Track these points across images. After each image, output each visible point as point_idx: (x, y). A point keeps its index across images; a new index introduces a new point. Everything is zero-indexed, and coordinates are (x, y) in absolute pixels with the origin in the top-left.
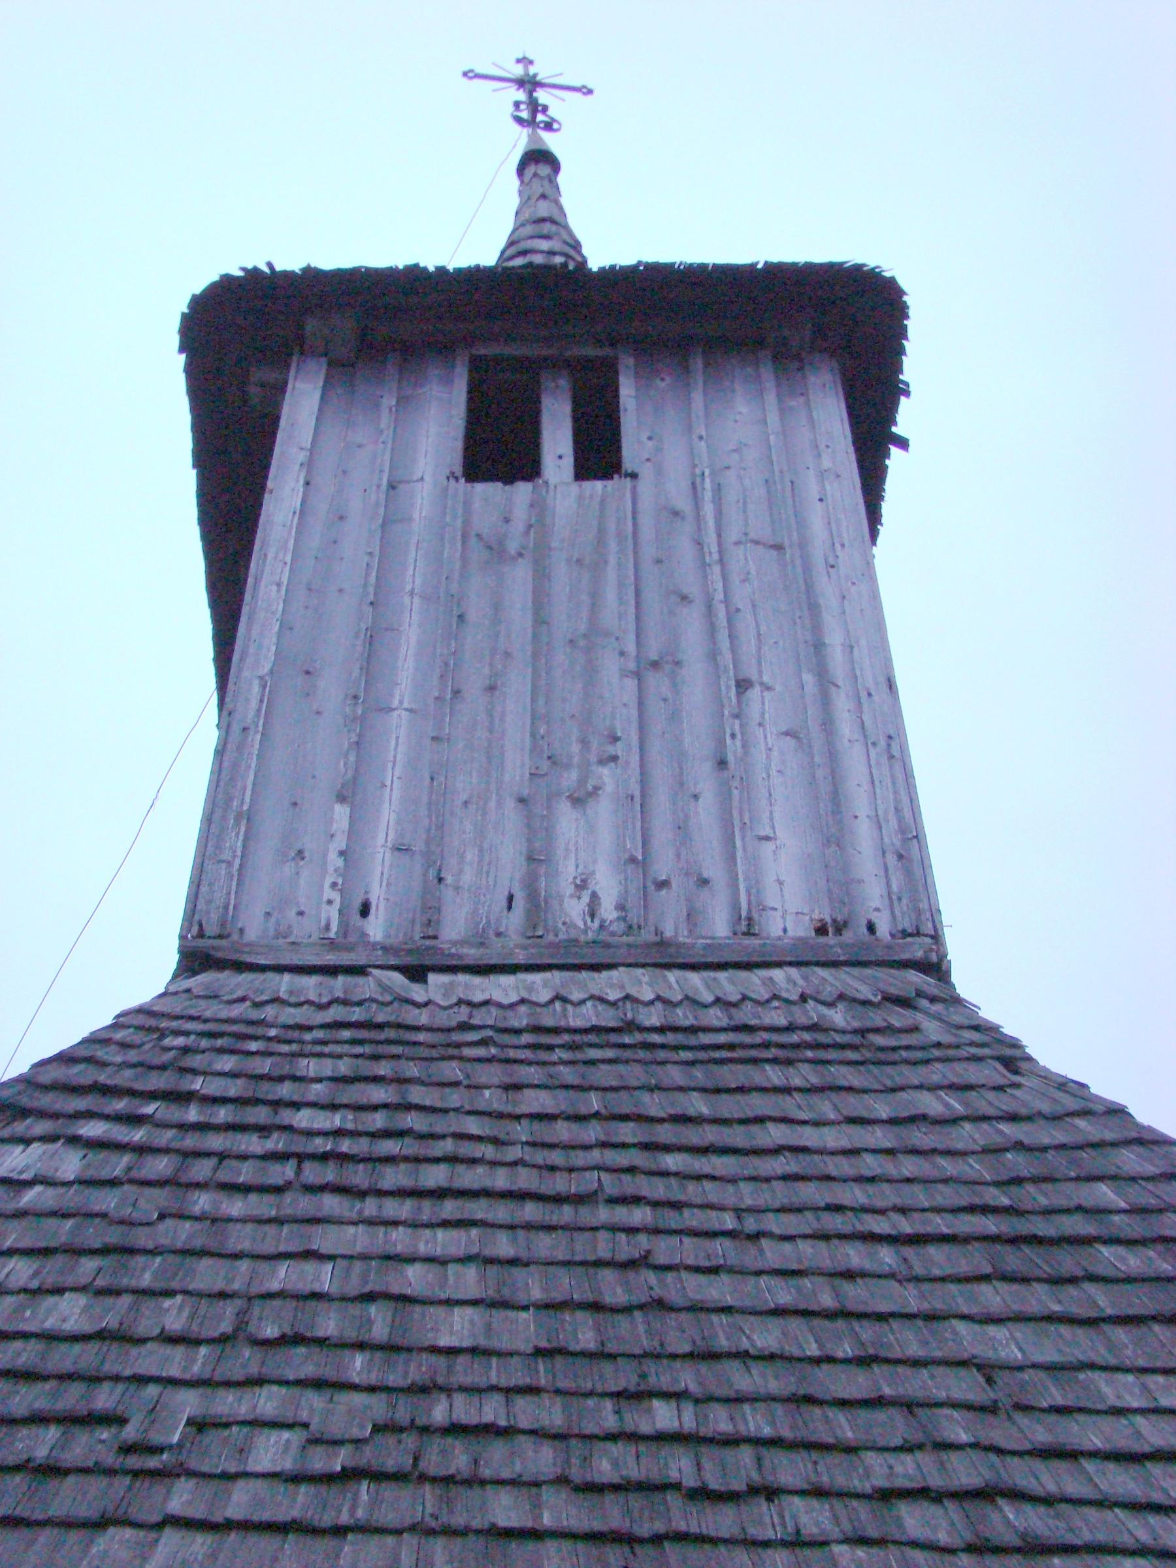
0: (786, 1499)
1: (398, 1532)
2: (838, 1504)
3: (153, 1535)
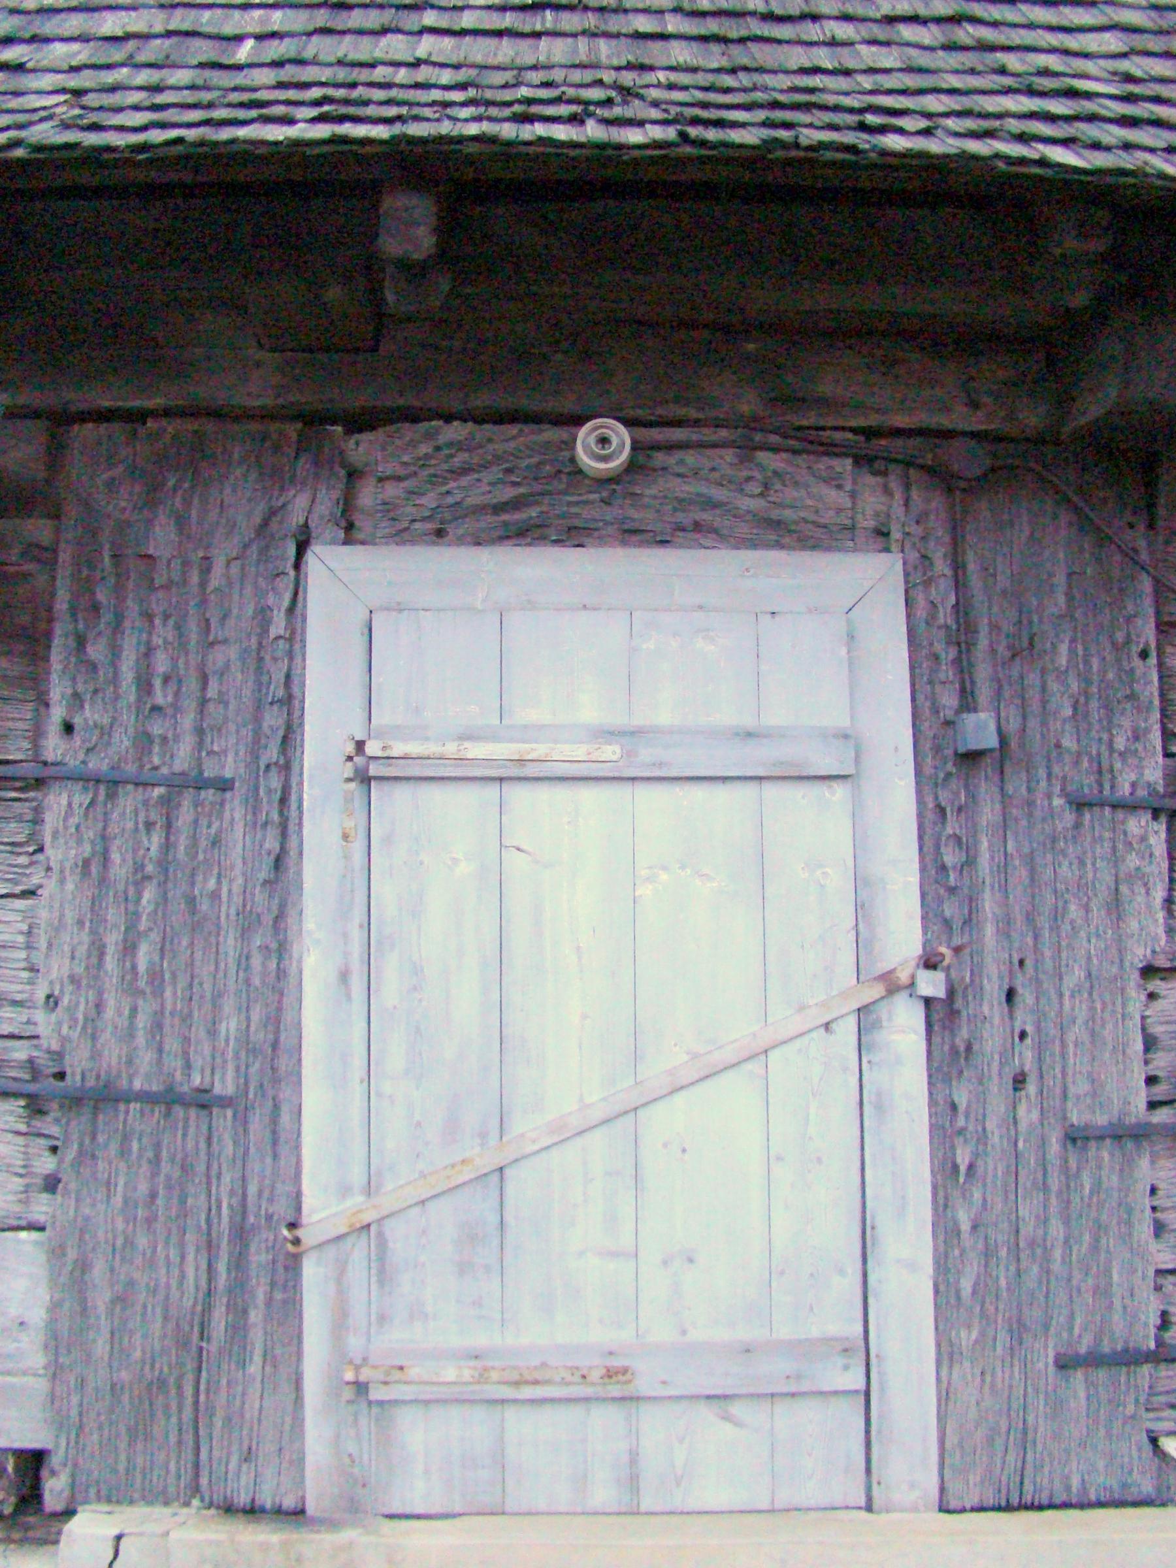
0: (825, 23)
1: (574, 35)
2: (859, 25)
3: (416, 38)
